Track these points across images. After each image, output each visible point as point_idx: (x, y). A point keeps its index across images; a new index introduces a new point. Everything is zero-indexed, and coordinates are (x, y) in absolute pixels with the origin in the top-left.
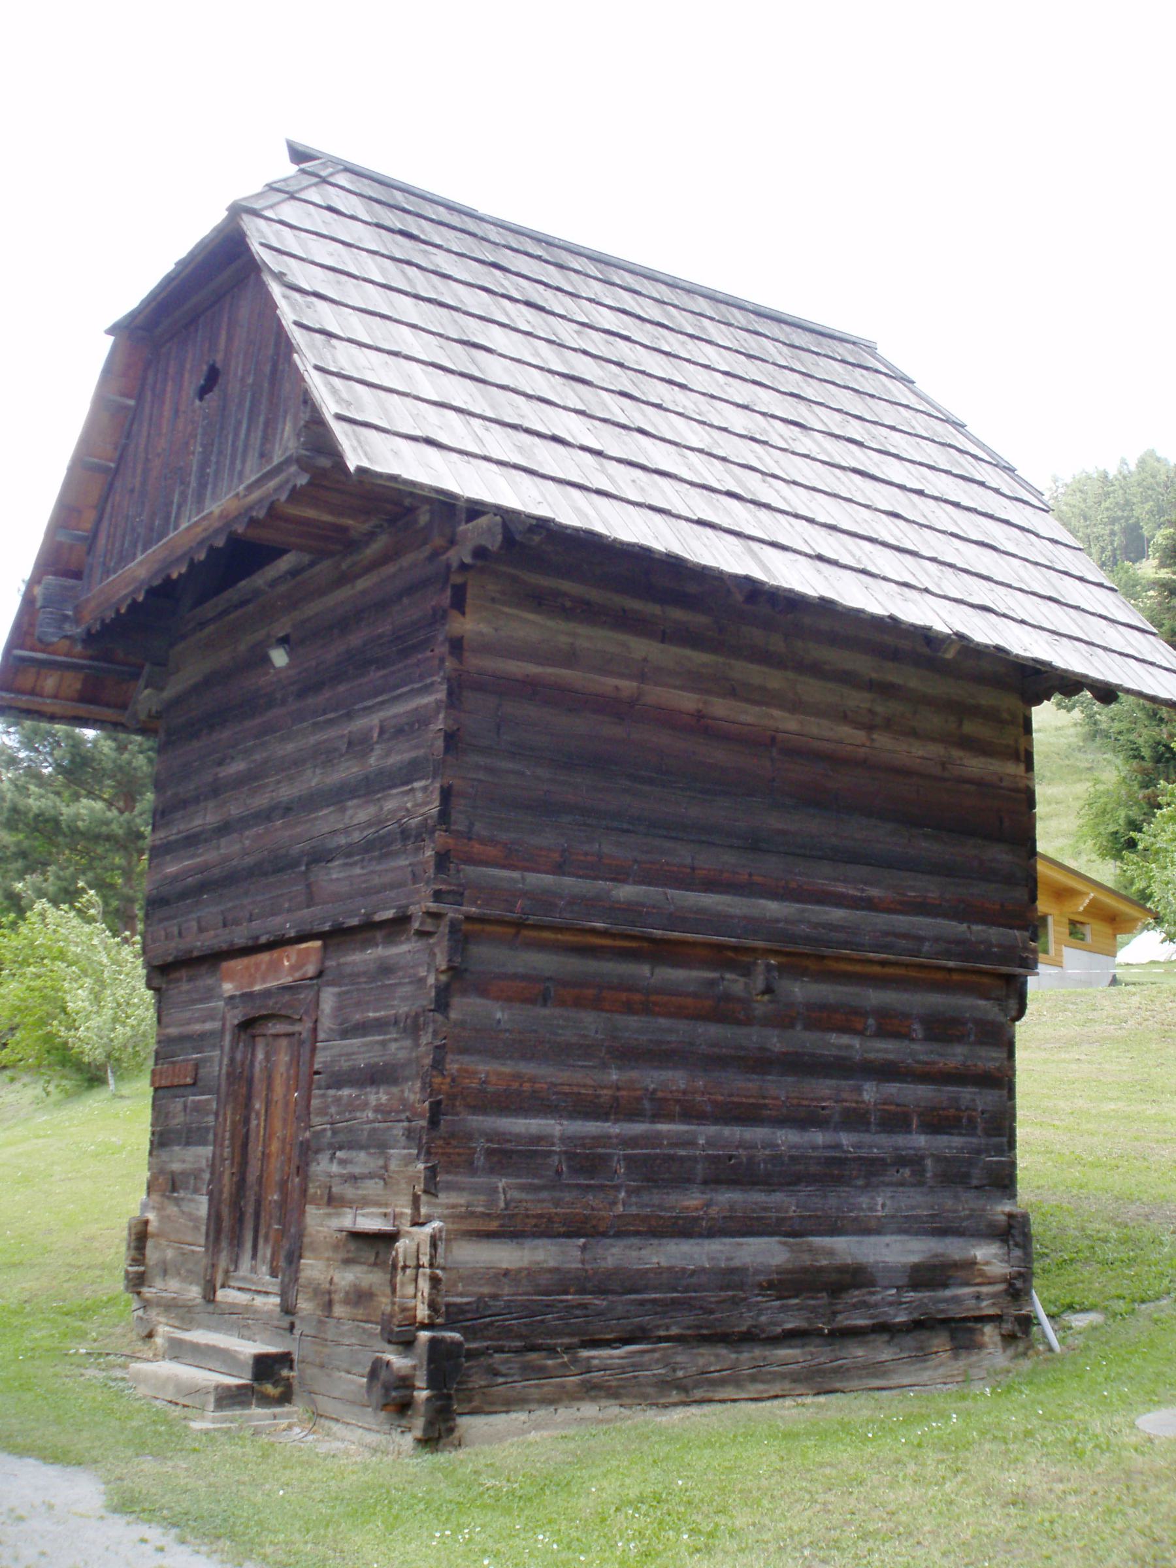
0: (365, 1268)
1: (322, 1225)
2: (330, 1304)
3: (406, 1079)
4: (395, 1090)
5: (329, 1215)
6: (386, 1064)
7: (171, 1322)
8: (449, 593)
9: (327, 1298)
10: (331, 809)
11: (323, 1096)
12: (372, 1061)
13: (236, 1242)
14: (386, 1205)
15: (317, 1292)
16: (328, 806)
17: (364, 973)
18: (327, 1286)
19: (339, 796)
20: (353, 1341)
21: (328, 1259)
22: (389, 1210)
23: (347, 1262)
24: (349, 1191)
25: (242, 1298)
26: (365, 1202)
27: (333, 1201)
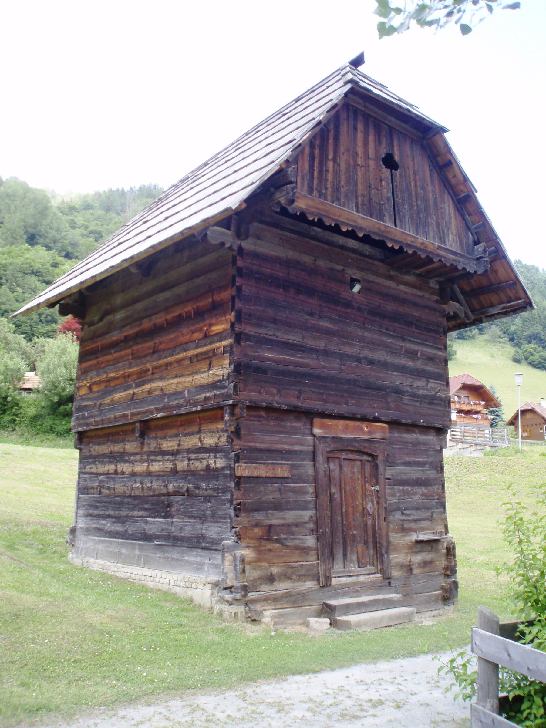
0: (427, 553)
1: (400, 540)
2: (411, 570)
3: (435, 485)
4: (430, 488)
5: (404, 536)
6: (425, 479)
7: (273, 607)
8: (233, 313)
9: (409, 568)
10: (399, 374)
11: (198, 488)
12: (419, 477)
13: (332, 555)
14: (433, 529)
15: (402, 566)
16: (398, 372)
17: (411, 443)
18: (408, 563)
19: (402, 369)
20: (425, 580)
21: (406, 553)
22: (435, 531)
23: (417, 553)
24: (413, 525)
25: (344, 580)
26: (422, 529)
27: (404, 530)
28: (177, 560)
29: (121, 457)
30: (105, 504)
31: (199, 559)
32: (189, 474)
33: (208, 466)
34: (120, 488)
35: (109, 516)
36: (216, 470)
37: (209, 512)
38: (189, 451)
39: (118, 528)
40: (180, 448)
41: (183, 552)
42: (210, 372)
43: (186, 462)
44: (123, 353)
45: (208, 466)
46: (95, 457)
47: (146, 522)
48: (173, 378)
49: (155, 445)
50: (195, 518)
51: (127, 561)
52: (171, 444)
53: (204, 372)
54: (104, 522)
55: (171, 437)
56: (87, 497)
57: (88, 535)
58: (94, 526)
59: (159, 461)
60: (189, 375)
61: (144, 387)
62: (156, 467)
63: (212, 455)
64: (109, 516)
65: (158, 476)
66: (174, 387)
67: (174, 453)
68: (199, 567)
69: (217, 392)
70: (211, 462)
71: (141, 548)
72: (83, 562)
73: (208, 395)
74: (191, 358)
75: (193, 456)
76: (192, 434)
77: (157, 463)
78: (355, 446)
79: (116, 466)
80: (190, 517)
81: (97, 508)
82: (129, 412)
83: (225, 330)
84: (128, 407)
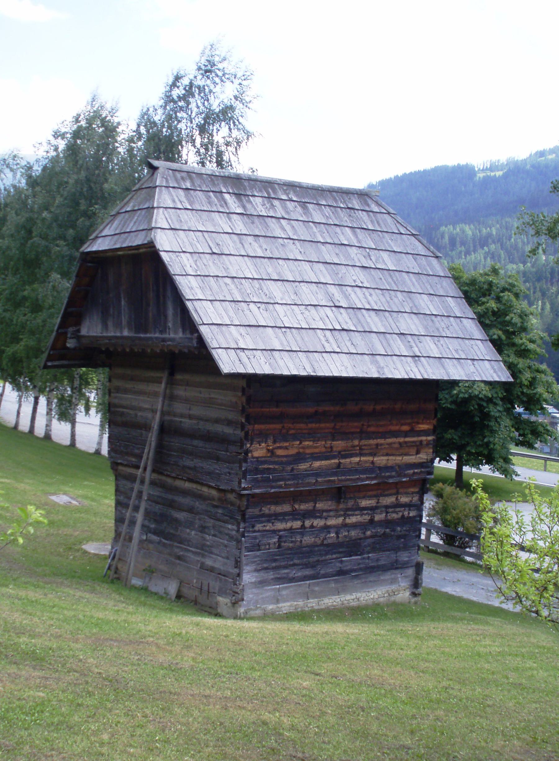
28: (375, 581)
29: (312, 514)
30: (288, 556)
31: (393, 576)
32: (387, 523)
33: (403, 516)
34: (308, 540)
35: (294, 565)
36: (409, 518)
37: (402, 545)
38: (387, 507)
39: (308, 572)
40: (379, 505)
41: (379, 575)
42: (418, 456)
43: (384, 514)
44: (323, 425)
45: (403, 516)
46: (270, 516)
47: (342, 562)
48: (383, 455)
49: (352, 503)
50: (389, 551)
51: (319, 595)
52: (370, 502)
53: (412, 455)
54: (286, 571)
55: (368, 497)
56: (258, 553)
57: (263, 587)
58: (272, 577)
59: (356, 515)
60: (399, 455)
61: (352, 459)
62: (353, 520)
63: (407, 509)
64: (294, 565)
65: (354, 526)
66: (384, 462)
67: (373, 509)
68: (394, 581)
69: (423, 470)
70: (406, 513)
71: (336, 581)
72: (533, 669)
73: (416, 471)
74: (400, 443)
75: (390, 510)
76: (391, 495)
77: (355, 517)
78: (308, 483)
79: (304, 522)
80: (384, 551)
81: (275, 560)
82: (336, 478)
83: (429, 429)
84: (335, 474)
